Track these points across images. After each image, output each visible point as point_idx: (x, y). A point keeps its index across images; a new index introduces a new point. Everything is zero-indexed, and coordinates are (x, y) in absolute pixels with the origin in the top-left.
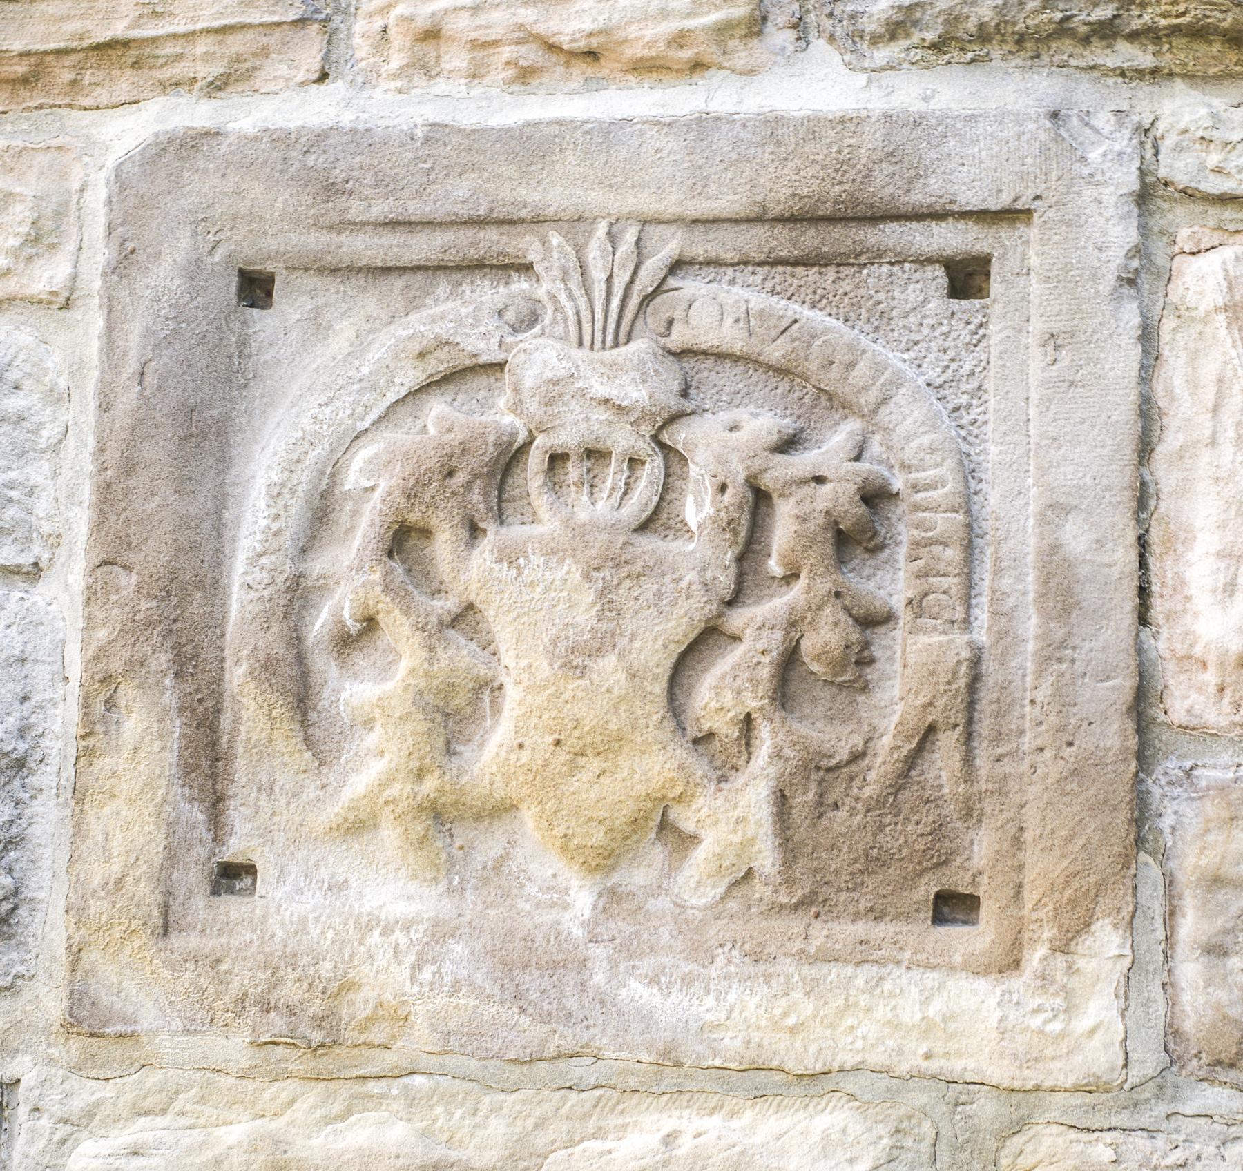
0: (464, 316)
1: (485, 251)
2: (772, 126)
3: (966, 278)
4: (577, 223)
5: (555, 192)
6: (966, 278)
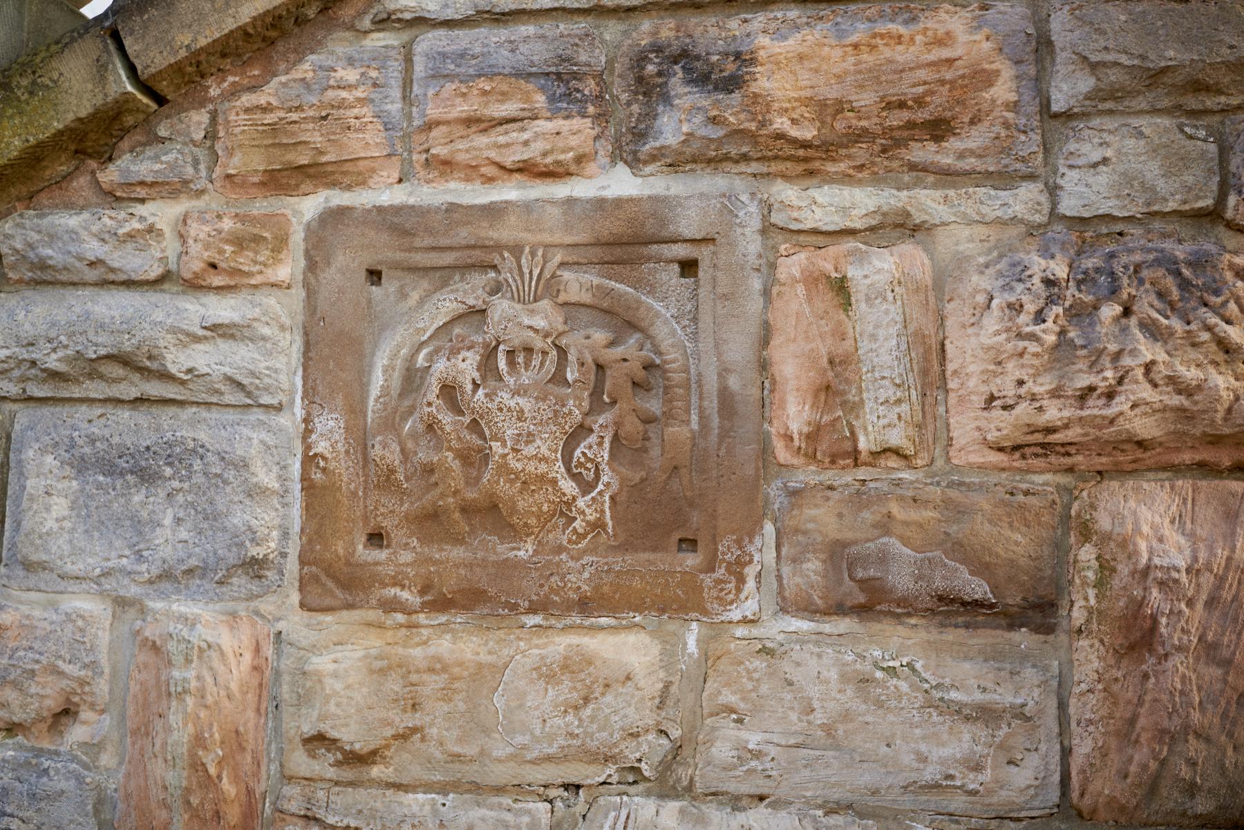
0: (472, 290)
1: (479, 259)
2: (600, 204)
3: (688, 267)
4: (517, 250)
5: (505, 233)
6: (688, 267)
